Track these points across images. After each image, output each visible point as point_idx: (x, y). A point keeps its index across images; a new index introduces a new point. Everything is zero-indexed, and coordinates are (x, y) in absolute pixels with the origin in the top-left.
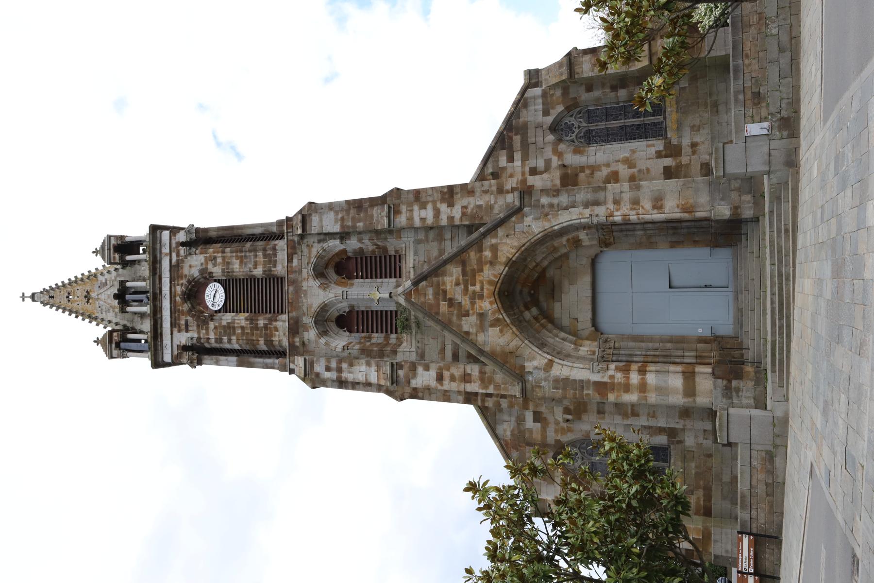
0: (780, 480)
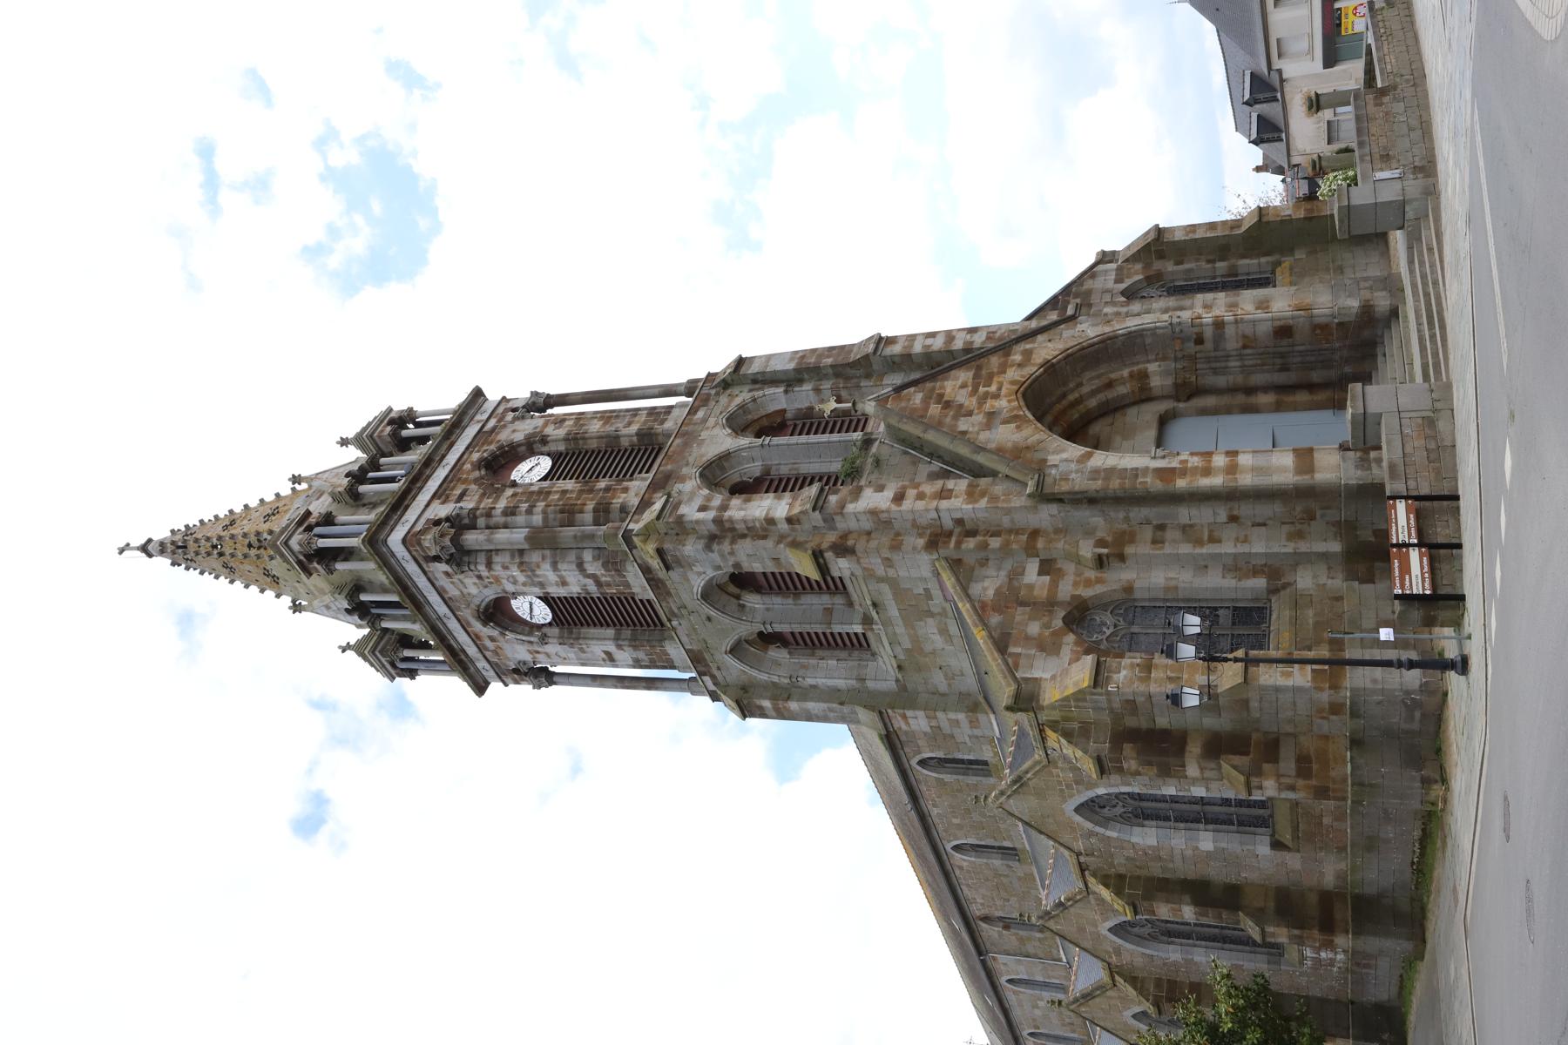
0: (1448, 443)
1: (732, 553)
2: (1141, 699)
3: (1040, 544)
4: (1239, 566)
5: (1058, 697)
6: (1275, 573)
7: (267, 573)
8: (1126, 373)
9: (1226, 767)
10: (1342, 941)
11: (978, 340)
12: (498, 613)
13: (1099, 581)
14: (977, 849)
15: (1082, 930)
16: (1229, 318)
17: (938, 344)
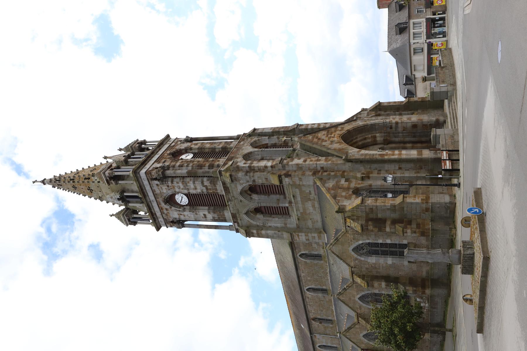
1: (253, 176)
2: (374, 208)
3: (346, 174)
5: (351, 208)
7: (89, 189)
8: (370, 136)
12: (170, 200)
13: (362, 183)
15: (350, 299)
16: (400, 121)
17: (316, 126)
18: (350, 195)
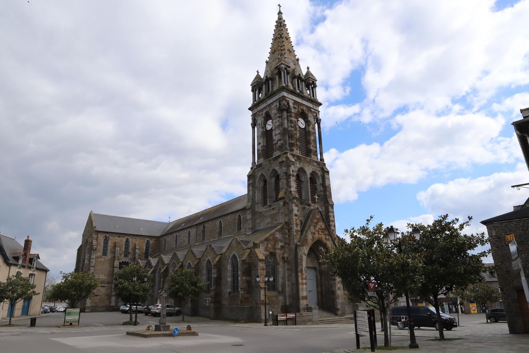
3: (287, 246)
4: (283, 285)
6: (283, 292)
7: (275, 51)
9: (245, 284)
10: (212, 305)
11: (332, 228)
12: (268, 117)
14: (221, 226)
17: (331, 219)
18: (269, 251)
